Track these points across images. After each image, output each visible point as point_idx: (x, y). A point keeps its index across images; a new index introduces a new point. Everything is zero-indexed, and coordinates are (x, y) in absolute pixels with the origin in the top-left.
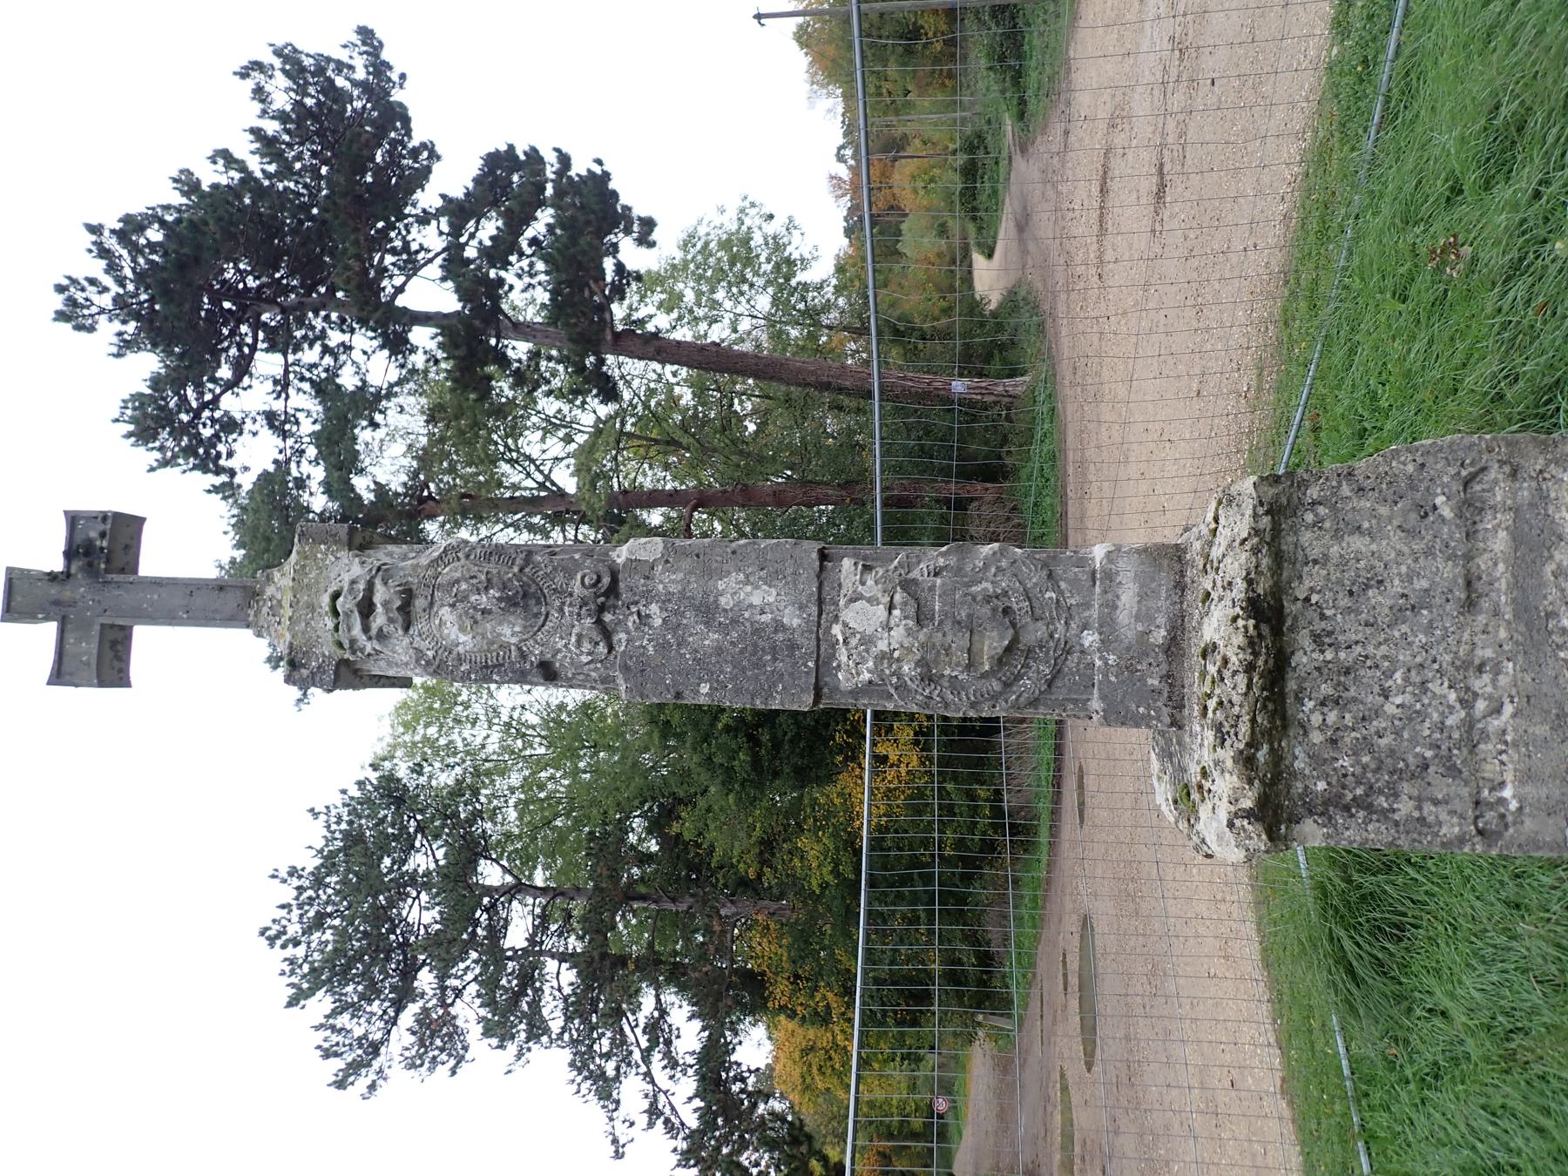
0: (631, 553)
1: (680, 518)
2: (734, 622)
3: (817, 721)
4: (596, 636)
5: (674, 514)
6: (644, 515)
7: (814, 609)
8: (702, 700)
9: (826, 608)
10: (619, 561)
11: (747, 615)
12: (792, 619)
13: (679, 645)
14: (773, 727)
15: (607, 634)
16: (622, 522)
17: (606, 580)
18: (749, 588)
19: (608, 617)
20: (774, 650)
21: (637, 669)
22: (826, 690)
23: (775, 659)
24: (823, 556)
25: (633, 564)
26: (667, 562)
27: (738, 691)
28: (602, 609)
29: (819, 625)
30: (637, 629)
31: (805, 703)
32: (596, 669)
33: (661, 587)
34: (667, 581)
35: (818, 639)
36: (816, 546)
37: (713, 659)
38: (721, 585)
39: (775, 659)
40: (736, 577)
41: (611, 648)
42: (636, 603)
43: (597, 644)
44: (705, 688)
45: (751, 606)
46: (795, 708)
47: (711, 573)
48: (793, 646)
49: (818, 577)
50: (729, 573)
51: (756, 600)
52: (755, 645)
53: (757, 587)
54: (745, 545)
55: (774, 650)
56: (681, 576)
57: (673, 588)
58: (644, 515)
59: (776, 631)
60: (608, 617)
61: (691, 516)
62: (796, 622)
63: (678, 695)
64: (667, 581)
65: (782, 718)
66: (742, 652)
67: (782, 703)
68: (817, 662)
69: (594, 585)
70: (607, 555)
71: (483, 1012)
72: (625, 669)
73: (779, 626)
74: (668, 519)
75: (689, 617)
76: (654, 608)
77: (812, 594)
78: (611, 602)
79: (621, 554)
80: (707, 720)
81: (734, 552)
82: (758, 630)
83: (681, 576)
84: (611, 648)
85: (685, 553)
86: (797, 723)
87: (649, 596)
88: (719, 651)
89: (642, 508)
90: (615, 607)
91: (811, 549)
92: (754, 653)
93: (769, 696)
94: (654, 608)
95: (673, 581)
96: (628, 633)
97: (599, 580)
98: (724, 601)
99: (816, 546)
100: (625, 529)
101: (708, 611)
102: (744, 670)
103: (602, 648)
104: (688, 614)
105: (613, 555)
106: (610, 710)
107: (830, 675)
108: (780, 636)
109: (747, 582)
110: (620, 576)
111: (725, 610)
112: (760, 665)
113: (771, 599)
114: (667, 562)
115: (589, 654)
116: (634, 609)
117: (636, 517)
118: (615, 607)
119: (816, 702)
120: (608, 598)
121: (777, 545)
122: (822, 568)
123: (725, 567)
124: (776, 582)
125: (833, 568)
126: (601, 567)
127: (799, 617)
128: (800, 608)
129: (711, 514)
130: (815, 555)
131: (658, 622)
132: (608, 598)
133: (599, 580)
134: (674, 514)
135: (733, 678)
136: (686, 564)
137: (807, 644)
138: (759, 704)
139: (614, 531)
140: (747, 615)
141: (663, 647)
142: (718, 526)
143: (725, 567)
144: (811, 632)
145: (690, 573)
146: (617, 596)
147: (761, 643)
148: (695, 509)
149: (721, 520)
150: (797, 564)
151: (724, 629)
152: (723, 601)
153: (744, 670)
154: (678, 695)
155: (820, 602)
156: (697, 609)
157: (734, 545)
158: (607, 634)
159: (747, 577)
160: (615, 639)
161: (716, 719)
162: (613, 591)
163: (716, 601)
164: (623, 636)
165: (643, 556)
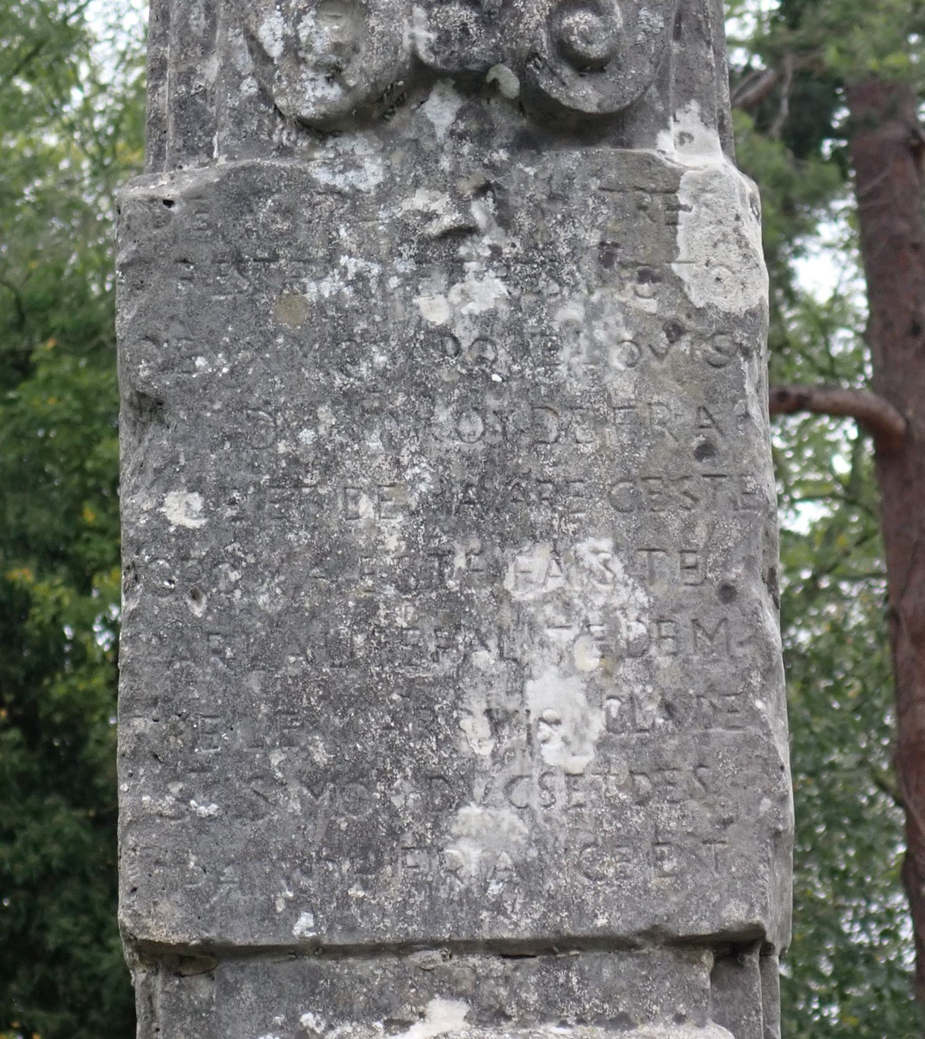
0: (702, 188)
1: (832, 370)
2: (453, 613)
3: (60, 956)
4: (366, 68)
5: (843, 341)
6: (833, 228)
7: (521, 924)
8: (135, 503)
9: (529, 974)
10: (666, 141)
11: (484, 658)
12: (479, 840)
13: (349, 398)
14: (29, 784)
15: (375, 110)
16: (801, 142)
17: (586, 96)
18: (589, 660)
19: (441, 111)
20: (352, 774)
21: (244, 241)
22: (204, 989)
23: (315, 780)
24: (735, 949)
25: (657, 199)
26: (675, 331)
27: (181, 639)
28: (473, 85)
29: (461, 947)
30: (402, 228)
31: (150, 911)
32: (231, 76)
33: (573, 311)
34: (598, 336)
35: (404, 948)
36: (774, 918)
37: (299, 538)
38: (595, 549)
39: (315, 780)
40: (629, 604)
41: (319, 129)
42: (504, 220)
43: (334, 74)
44: (183, 510)
45: (520, 673)
46: (129, 872)
47: (641, 504)
48: (370, 848)
49: (652, 934)
50: (647, 579)
51: (547, 692)
52: (367, 698)
53: (595, 693)
54: (758, 637)
55: (352, 774)
56: (622, 386)
57: (571, 361)
58: (833, 228)
59: (427, 779)
60: (441, 111)
61: (838, 413)
62: (467, 854)
63: (150, 407)
64: (598, 336)
65: (66, 819)
66: (335, 647)
67: (143, 820)
68: (319, 949)
69: (564, 50)
70: (687, 94)
71: (79, 814)
72: (242, 193)
73: (446, 789)
74: (823, 322)
75: (459, 433)
76: (487, 291)
77: (579, 910)
78: (506, 122)
79: (694, 150)
80: (42, 521)
81: (728, 592)
82: (427, 707)
83: (622, 386)
84: (319, 129)
85: (712, 392)
86: (48, 879)
87: (534, 267)
88: (337, 557)
89: (862, 217)
90: (484, 138)
91: (761, 897)
92: (334, 699)
93: (167, 765)
94: (487, 291)
95: (598, 359)
96: (386, 193)
97: (586, 67)
98: (532, 570)
99: (774, 918)
100: (775, 155)
101: (491, 502)
102: (264, 659)
103: (316, 95)
104: (473, 425)
105: (689, 117)
106: (51, 140)
107: (267, 1005)
108: (406, 797)
109: (613, 653)
110: (605, 151)
111: (496, 573)
112: (289, 717)
113: (552, 753)
114: (675, 331)
115: (293, 46)
116: (480, 212)
117: (819, 196)
118: (484, 138)
119: (159, 956)
120: (519, 105)
121: (769, 764)
122: (687, 945)
123: (668, 563)
124: (620, 764)
125: (689, 991)
126: (638, 71)
127: (490, 869)
128: (523, 869)
129: (850, 493)
130: (735, 914)
131: (435, 308)
132: (519, 105)
133: (586, 67)
134: (843, 341)
135: (229, 620)
136: (672, 407)
137: (384, 905)
138: (132, 728)
139: (760, 111)
140: (484, 658)
141: (338, 334)
142: (806, 517)
143: (668, 563)
144: (432, 917)
145: (638, 424)
146: (527, 143)
147: (374, 721)
148: (869, 424)
149: (830, 531)
150: (697, 846)
151: (422, 572)
152: (534, 560)
153: (264, 659)
154: (150, 407)
155: (551, 948)
156: (494, 461)
157: (758, 591)
158: (375, 110)
159: (637, 651)
160: (359, 145)
161: (51, 556)
162: (549, 124)
163: (531, 534)
164: (371, 174)
165: (692, 235)
